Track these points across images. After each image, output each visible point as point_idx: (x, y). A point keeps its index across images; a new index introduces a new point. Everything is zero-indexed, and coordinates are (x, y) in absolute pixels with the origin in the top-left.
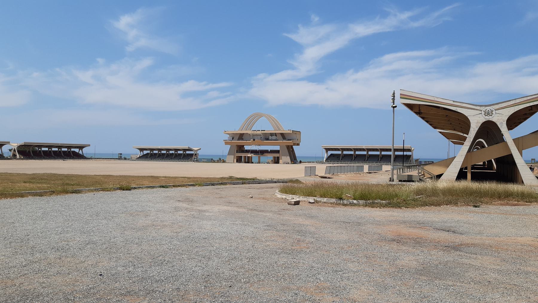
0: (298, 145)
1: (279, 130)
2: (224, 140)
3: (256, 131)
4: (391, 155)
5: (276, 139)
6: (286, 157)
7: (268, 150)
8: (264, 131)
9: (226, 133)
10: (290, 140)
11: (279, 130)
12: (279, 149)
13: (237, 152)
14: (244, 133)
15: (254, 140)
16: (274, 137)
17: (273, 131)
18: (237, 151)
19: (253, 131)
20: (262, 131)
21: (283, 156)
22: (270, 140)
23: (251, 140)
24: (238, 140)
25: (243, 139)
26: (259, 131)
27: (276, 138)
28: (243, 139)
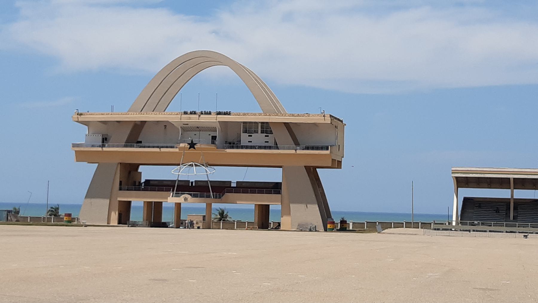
0: (337, 164)
1: (278, 113)
2: (74, 145)
3: (195, 113)
4: (144, 202)
5: (267, 144)
6: (303, 206)
7: (230, 182)
8: (226, 114)
9: (81, 118)
10: (322, 148)
11: (278, 113)
12: (281, 181)
13: (120, 189)
14: (145, 122)
15: (192, 145)
16: (259, 138)
17: (260, 114)
18: (121, 183)
19: (185, 113)
20: (219, 113)
21: (294, 202)
22: (242, 147)
23: (182, 145)
24: (126, 146)
25: (141, 142)
26: (206, 113)
27: (267, 139)
28: (141, 142)
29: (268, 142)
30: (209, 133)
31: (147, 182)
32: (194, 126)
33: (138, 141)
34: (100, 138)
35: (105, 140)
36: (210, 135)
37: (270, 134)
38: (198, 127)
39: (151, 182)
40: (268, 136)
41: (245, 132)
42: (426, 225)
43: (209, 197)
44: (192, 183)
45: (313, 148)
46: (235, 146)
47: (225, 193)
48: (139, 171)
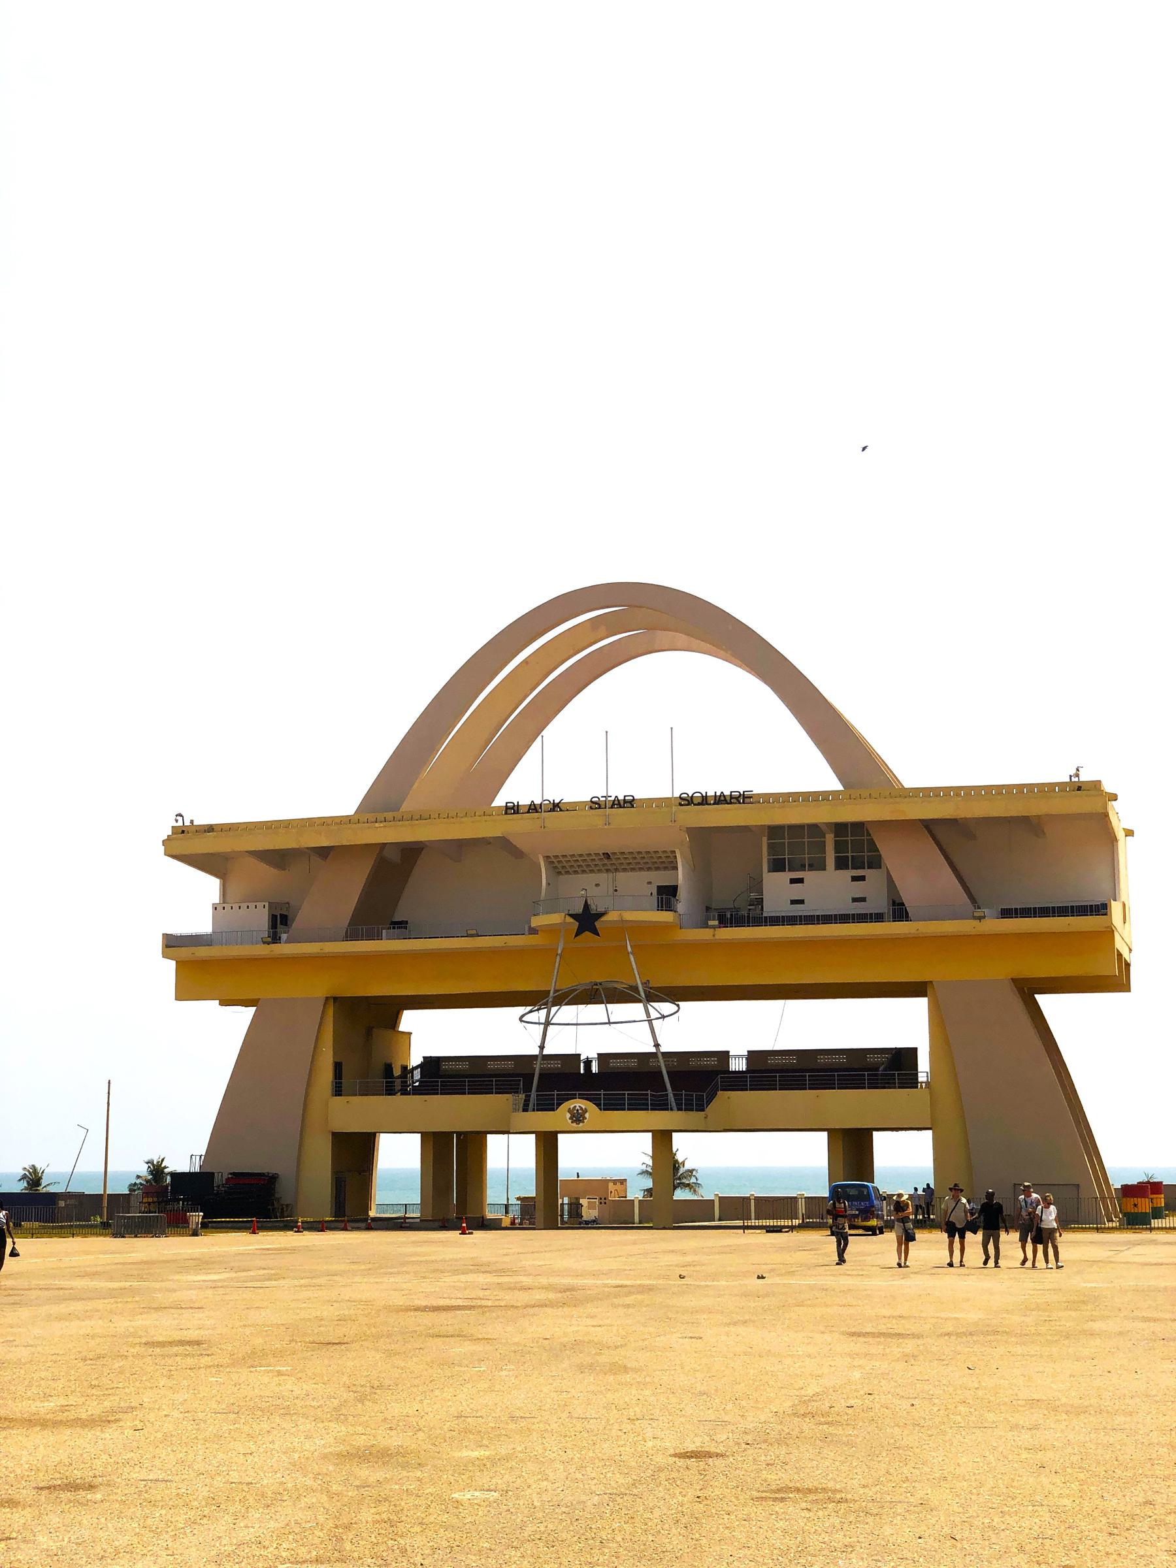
5: (859, 908)
27: (858, 889)
28: (402, 925)
29: (863, 900)
30: (646, 875)
31: (431, 1064)
32: (643, 850)
33: (392, 922)
34: (260, 917)
35: (281, 924)
36: (650, 883)
37: (812, 867)
38: (607, 856)
39: (444, 1066)
40: (862, 878)
41: (778, 866)
42: (468, 1294)
43: (662, 1105)
44: (588, 1063)
45: (1026, 913)
46: (362, 929)
47: (720, 1093)
48: (403, 1027)
